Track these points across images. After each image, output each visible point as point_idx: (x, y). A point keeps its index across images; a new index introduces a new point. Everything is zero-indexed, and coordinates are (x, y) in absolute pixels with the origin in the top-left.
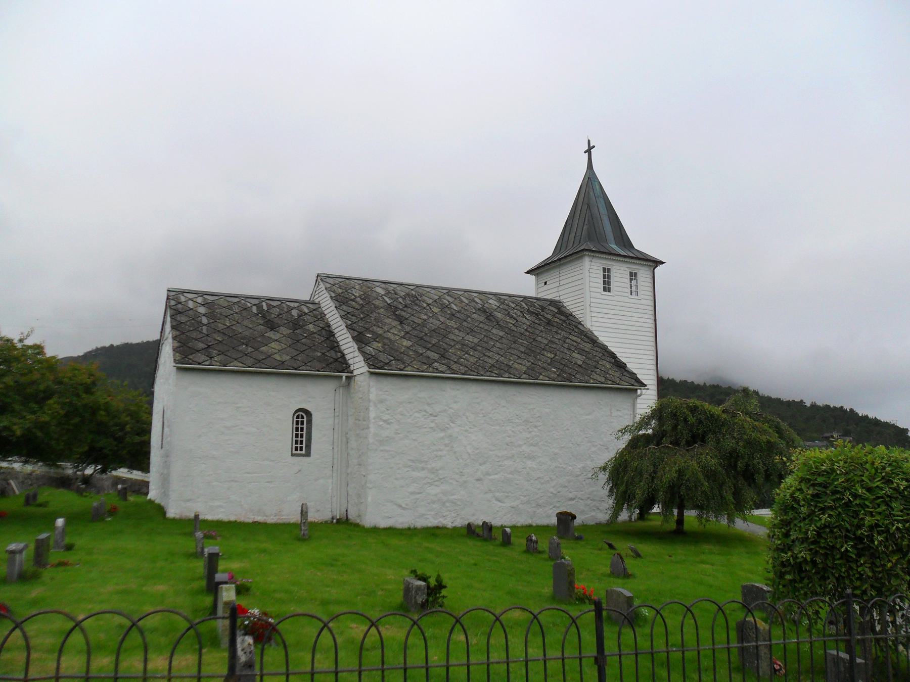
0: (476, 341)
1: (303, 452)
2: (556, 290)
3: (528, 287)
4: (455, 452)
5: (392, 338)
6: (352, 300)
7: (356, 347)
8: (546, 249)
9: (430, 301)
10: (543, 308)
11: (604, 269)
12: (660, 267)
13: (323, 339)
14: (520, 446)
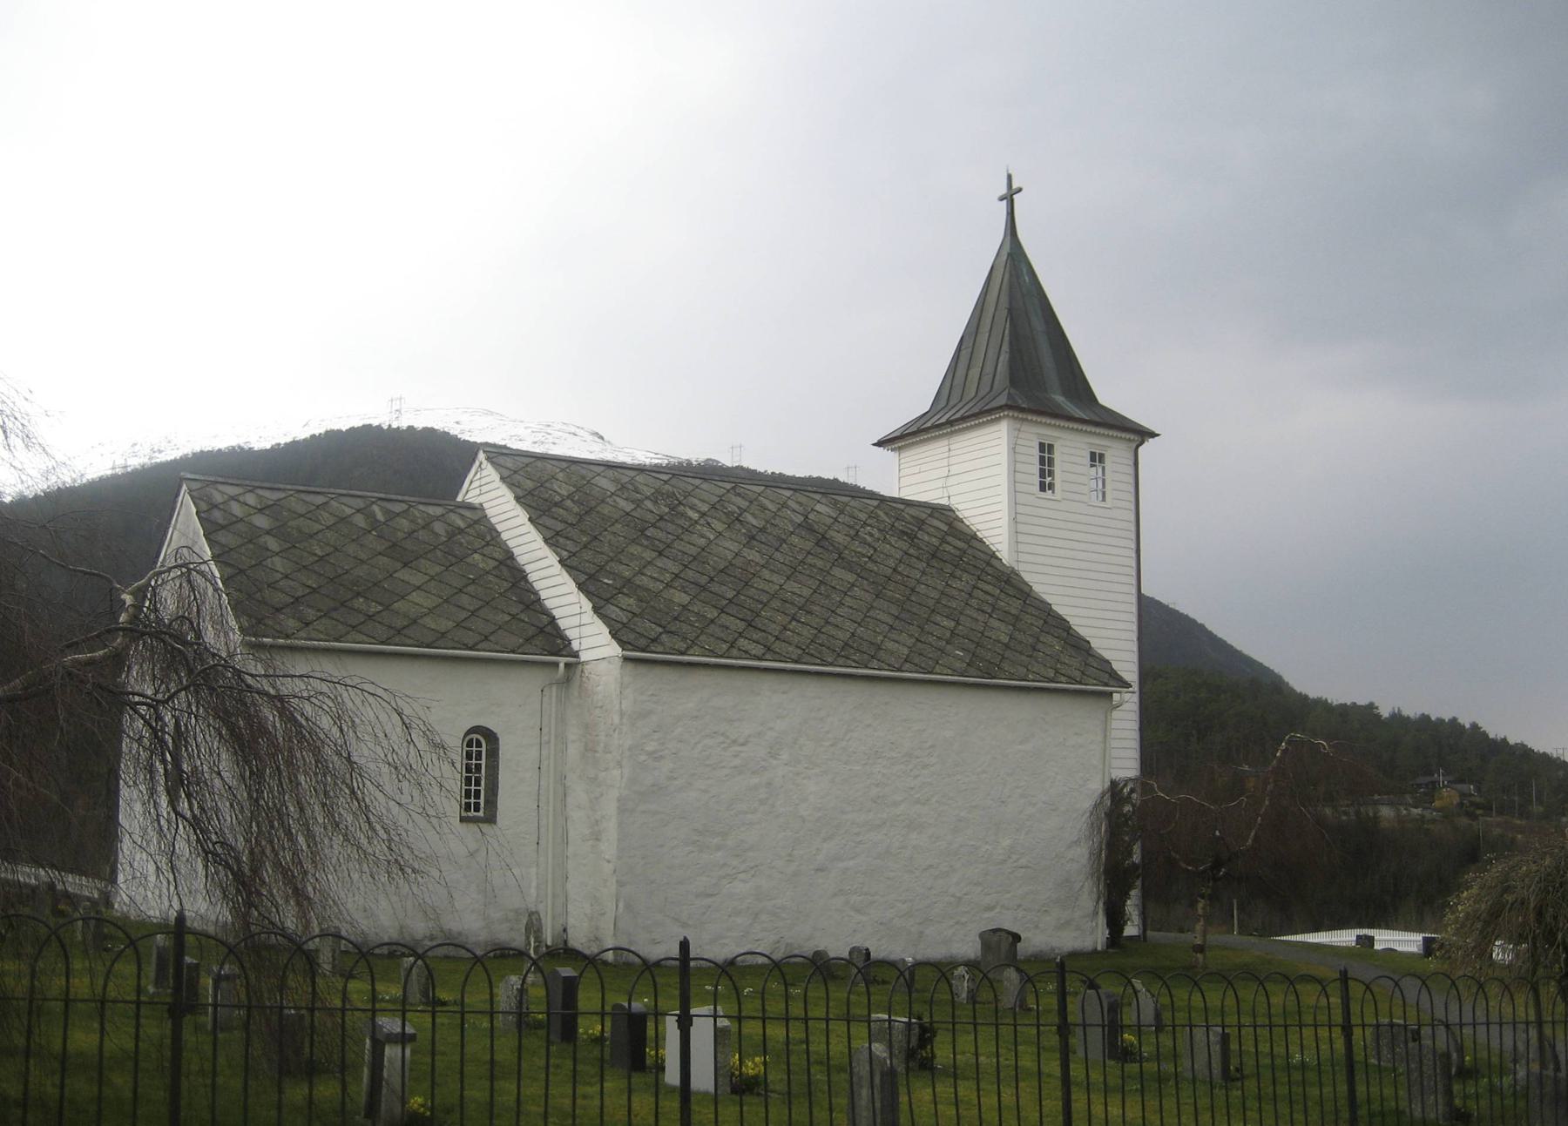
0: (806, 592)
1: (481, 814)
5: (652, 585)
6: (556, 504)
8: (918, 400)
9: (705, 508)
10: (921, 523)
11: (1042, 446)
13: (506, 585)
14: (896, 804)
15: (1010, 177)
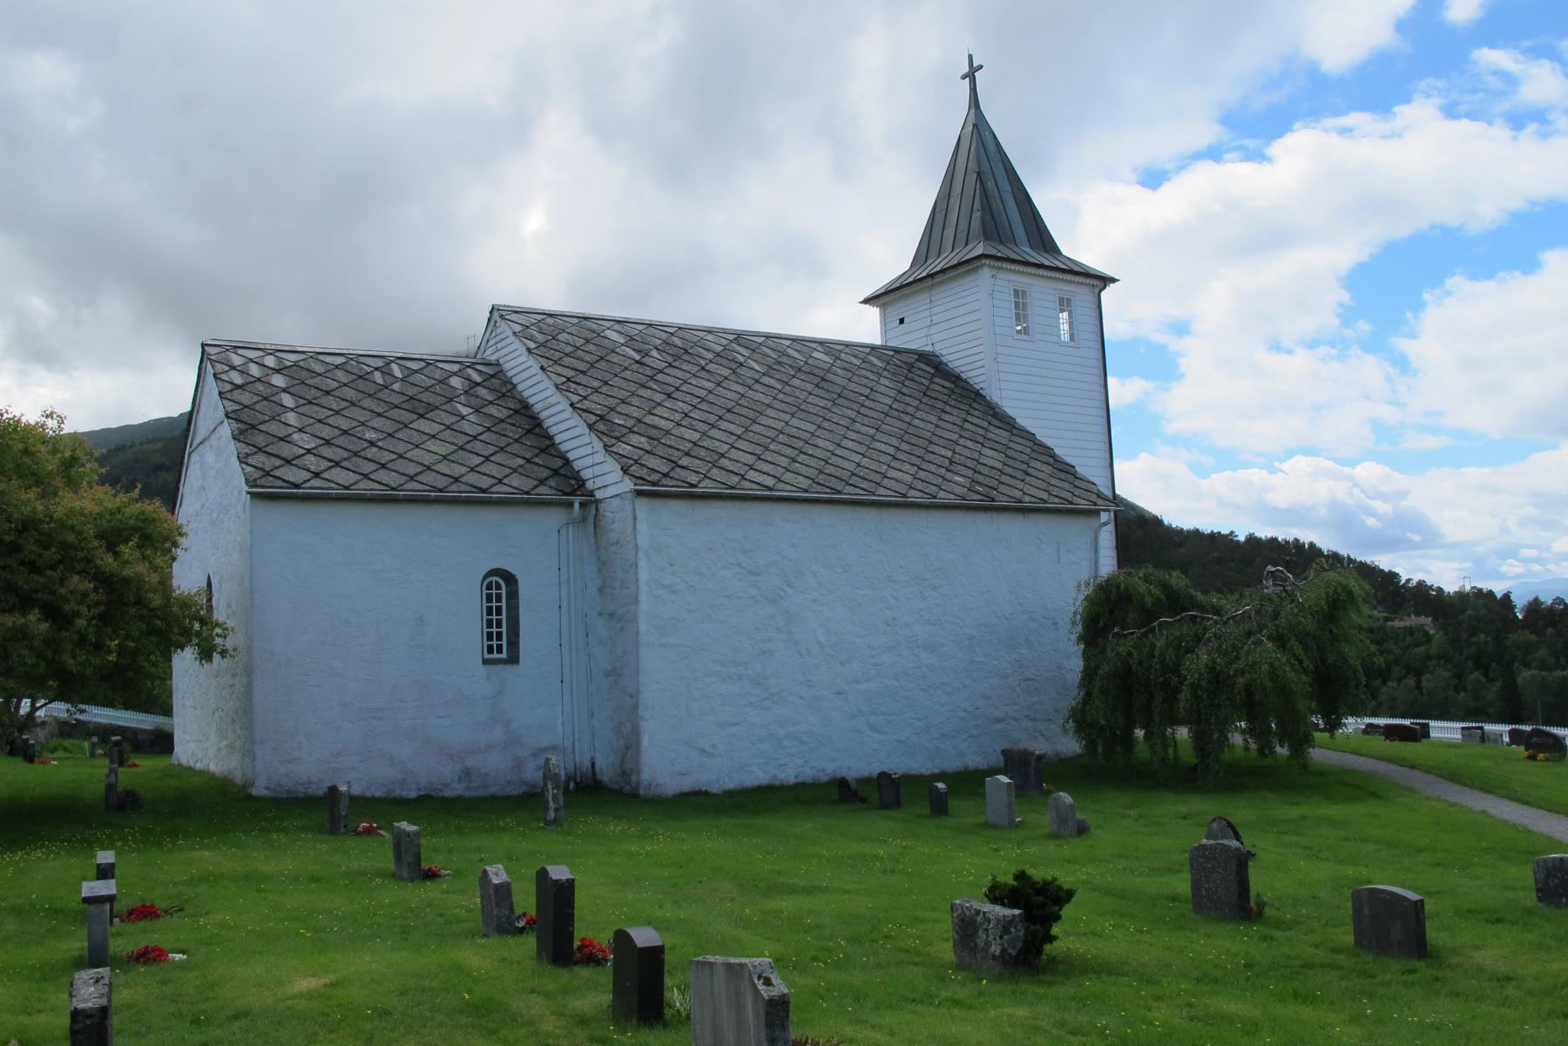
1: (504, 655)
2: (924, 332)
3: (866, 328)
4: (796, 643)
7: (598, 446)
8: (893, 256)
11: (1016, 292)
12: (1111, 288)
15: (970, 57)
